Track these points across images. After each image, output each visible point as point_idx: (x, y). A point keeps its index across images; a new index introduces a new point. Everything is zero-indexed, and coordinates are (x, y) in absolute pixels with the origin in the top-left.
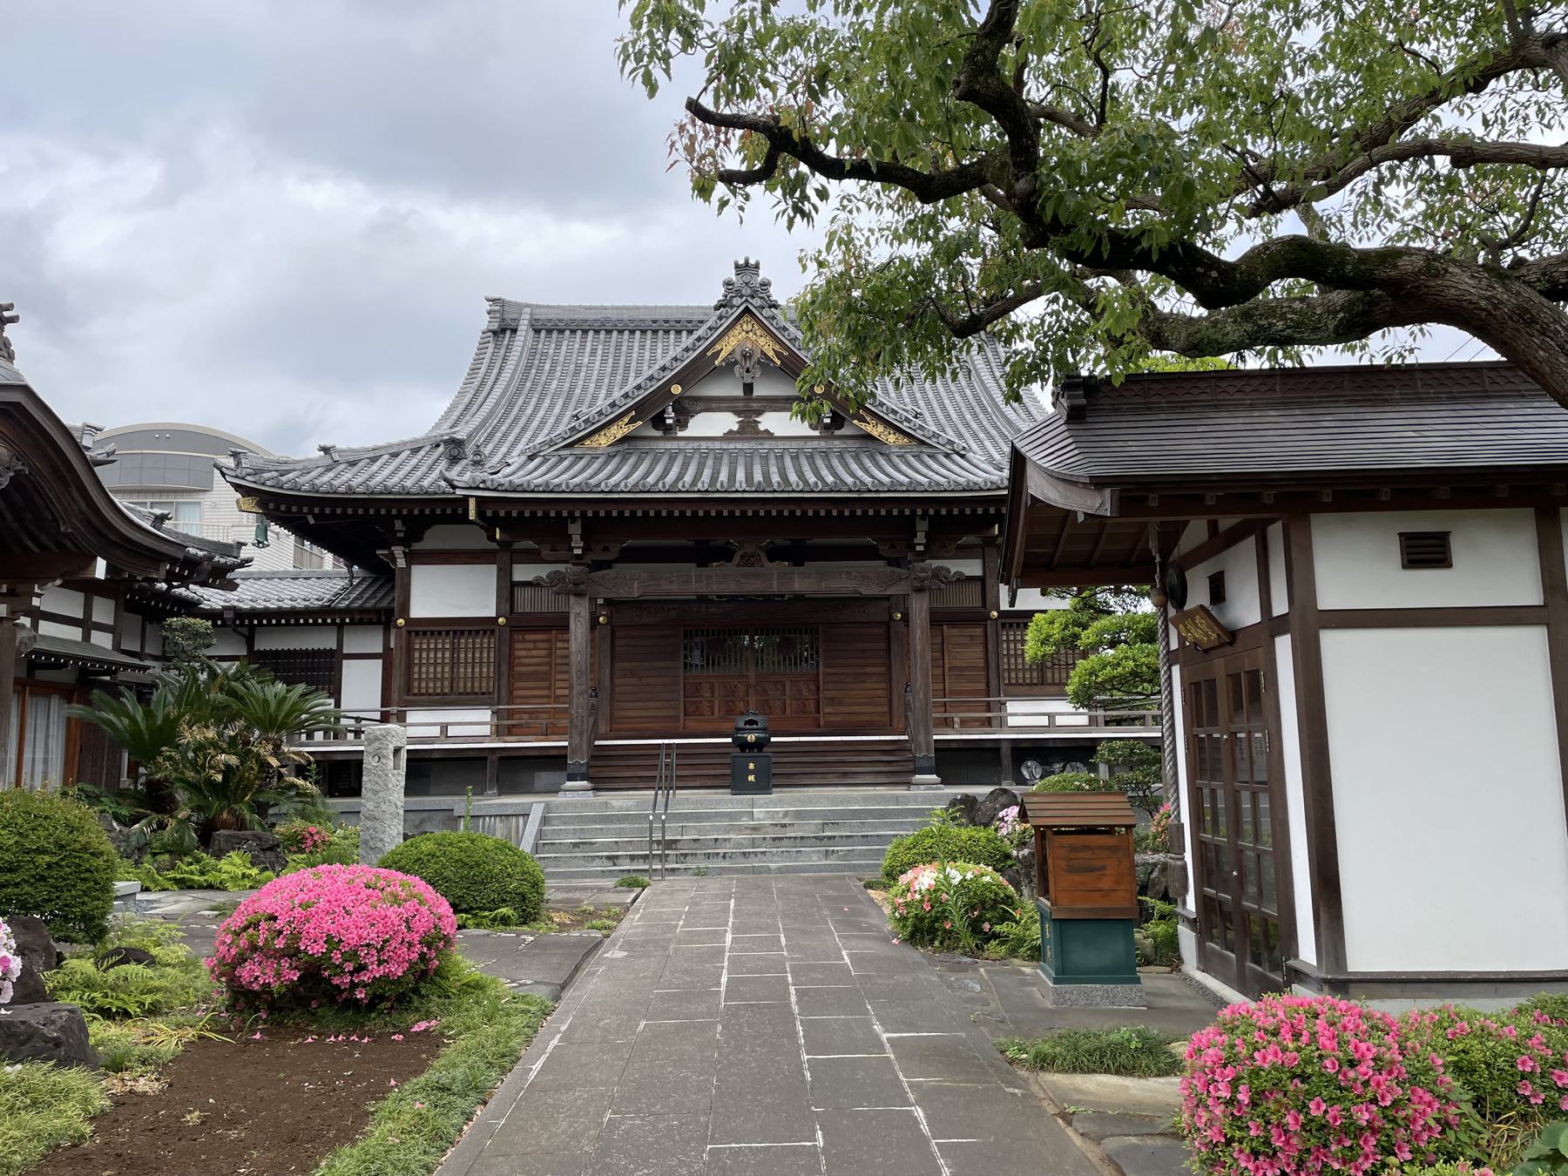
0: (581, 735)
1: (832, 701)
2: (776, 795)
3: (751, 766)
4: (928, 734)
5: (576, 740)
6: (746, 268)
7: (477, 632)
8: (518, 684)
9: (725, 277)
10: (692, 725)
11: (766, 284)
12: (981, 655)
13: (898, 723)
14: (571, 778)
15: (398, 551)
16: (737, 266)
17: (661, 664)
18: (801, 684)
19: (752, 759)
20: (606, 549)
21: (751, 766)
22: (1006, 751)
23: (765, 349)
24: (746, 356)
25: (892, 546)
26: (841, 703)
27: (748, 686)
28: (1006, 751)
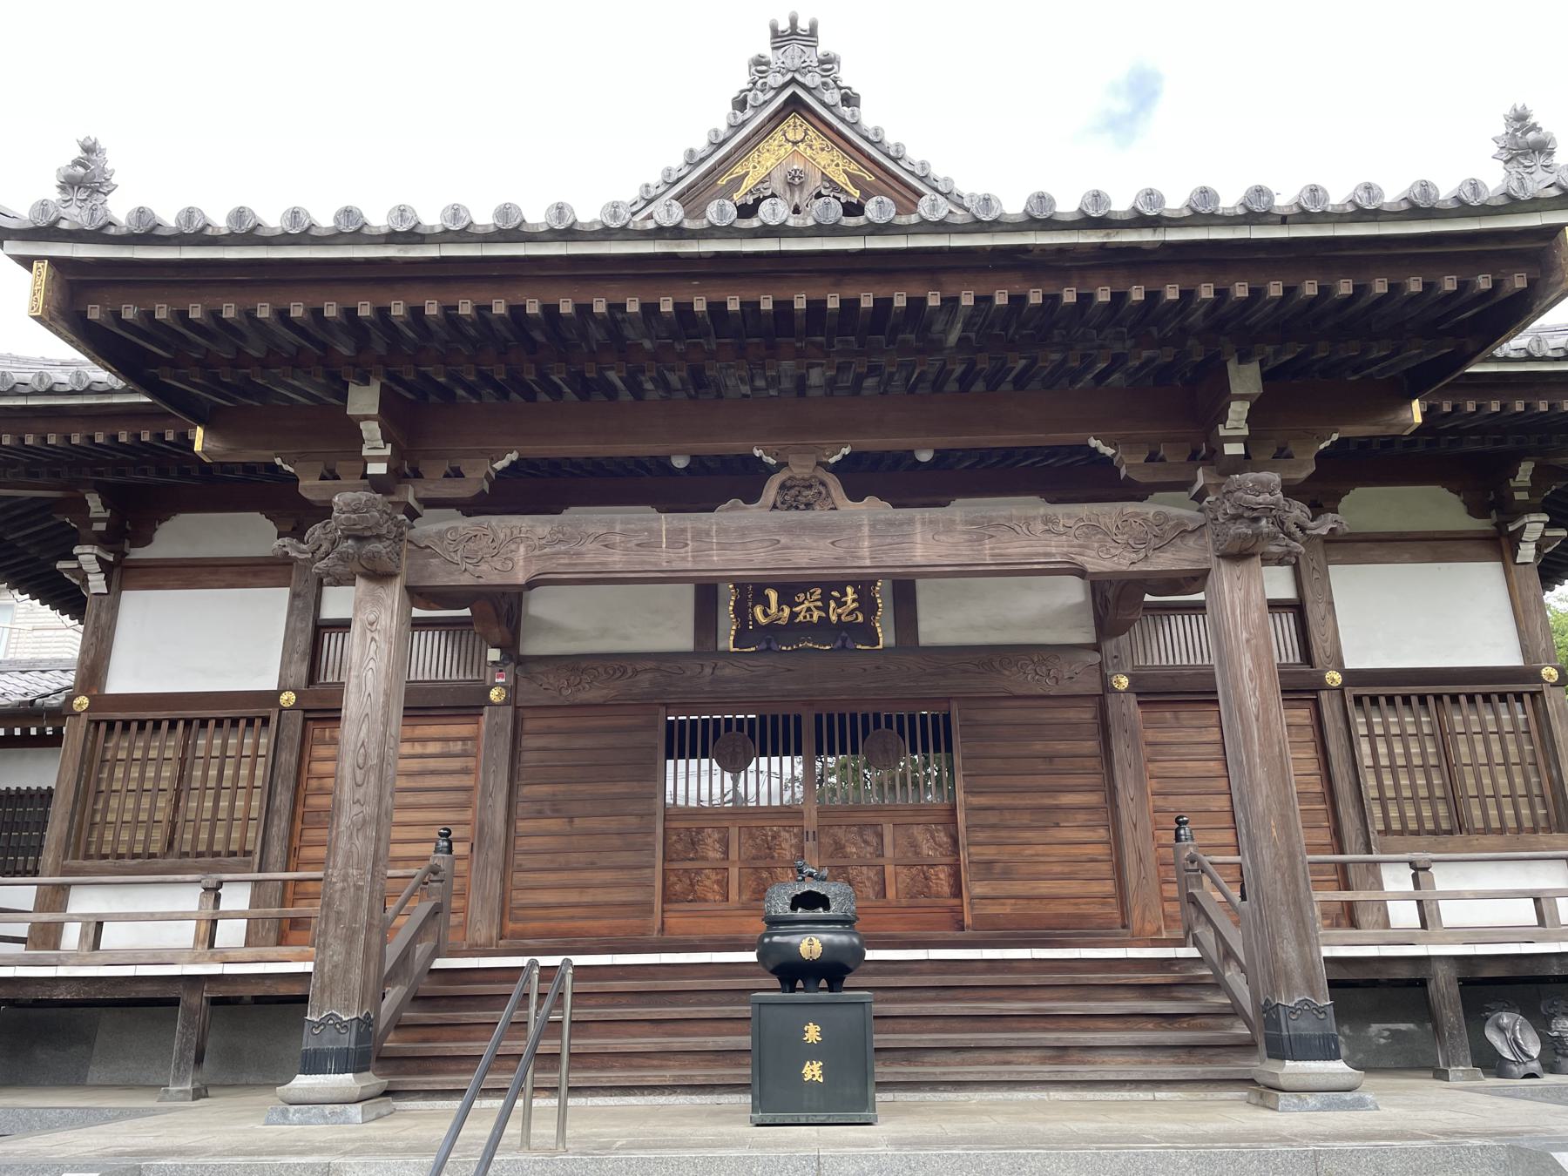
1: (986, 869)
3: (812, 1033)
4: (1305, 939)
5: (336, 952)
7: (235, 722)
9: (753, 54)
10: (679, 923)
11: (828, 61)
12: (1313, 767)
14: (314, 1063)
15: (87, 556)
16: (776, 34)
17: (620, 788)
18: (917, 832)
20: (457, 473)
21: (812, 1033)
22: (1444, 986)
23: (829, 172)
26: (1007, 875)
27: (802, 836)
28: (1444, 986)
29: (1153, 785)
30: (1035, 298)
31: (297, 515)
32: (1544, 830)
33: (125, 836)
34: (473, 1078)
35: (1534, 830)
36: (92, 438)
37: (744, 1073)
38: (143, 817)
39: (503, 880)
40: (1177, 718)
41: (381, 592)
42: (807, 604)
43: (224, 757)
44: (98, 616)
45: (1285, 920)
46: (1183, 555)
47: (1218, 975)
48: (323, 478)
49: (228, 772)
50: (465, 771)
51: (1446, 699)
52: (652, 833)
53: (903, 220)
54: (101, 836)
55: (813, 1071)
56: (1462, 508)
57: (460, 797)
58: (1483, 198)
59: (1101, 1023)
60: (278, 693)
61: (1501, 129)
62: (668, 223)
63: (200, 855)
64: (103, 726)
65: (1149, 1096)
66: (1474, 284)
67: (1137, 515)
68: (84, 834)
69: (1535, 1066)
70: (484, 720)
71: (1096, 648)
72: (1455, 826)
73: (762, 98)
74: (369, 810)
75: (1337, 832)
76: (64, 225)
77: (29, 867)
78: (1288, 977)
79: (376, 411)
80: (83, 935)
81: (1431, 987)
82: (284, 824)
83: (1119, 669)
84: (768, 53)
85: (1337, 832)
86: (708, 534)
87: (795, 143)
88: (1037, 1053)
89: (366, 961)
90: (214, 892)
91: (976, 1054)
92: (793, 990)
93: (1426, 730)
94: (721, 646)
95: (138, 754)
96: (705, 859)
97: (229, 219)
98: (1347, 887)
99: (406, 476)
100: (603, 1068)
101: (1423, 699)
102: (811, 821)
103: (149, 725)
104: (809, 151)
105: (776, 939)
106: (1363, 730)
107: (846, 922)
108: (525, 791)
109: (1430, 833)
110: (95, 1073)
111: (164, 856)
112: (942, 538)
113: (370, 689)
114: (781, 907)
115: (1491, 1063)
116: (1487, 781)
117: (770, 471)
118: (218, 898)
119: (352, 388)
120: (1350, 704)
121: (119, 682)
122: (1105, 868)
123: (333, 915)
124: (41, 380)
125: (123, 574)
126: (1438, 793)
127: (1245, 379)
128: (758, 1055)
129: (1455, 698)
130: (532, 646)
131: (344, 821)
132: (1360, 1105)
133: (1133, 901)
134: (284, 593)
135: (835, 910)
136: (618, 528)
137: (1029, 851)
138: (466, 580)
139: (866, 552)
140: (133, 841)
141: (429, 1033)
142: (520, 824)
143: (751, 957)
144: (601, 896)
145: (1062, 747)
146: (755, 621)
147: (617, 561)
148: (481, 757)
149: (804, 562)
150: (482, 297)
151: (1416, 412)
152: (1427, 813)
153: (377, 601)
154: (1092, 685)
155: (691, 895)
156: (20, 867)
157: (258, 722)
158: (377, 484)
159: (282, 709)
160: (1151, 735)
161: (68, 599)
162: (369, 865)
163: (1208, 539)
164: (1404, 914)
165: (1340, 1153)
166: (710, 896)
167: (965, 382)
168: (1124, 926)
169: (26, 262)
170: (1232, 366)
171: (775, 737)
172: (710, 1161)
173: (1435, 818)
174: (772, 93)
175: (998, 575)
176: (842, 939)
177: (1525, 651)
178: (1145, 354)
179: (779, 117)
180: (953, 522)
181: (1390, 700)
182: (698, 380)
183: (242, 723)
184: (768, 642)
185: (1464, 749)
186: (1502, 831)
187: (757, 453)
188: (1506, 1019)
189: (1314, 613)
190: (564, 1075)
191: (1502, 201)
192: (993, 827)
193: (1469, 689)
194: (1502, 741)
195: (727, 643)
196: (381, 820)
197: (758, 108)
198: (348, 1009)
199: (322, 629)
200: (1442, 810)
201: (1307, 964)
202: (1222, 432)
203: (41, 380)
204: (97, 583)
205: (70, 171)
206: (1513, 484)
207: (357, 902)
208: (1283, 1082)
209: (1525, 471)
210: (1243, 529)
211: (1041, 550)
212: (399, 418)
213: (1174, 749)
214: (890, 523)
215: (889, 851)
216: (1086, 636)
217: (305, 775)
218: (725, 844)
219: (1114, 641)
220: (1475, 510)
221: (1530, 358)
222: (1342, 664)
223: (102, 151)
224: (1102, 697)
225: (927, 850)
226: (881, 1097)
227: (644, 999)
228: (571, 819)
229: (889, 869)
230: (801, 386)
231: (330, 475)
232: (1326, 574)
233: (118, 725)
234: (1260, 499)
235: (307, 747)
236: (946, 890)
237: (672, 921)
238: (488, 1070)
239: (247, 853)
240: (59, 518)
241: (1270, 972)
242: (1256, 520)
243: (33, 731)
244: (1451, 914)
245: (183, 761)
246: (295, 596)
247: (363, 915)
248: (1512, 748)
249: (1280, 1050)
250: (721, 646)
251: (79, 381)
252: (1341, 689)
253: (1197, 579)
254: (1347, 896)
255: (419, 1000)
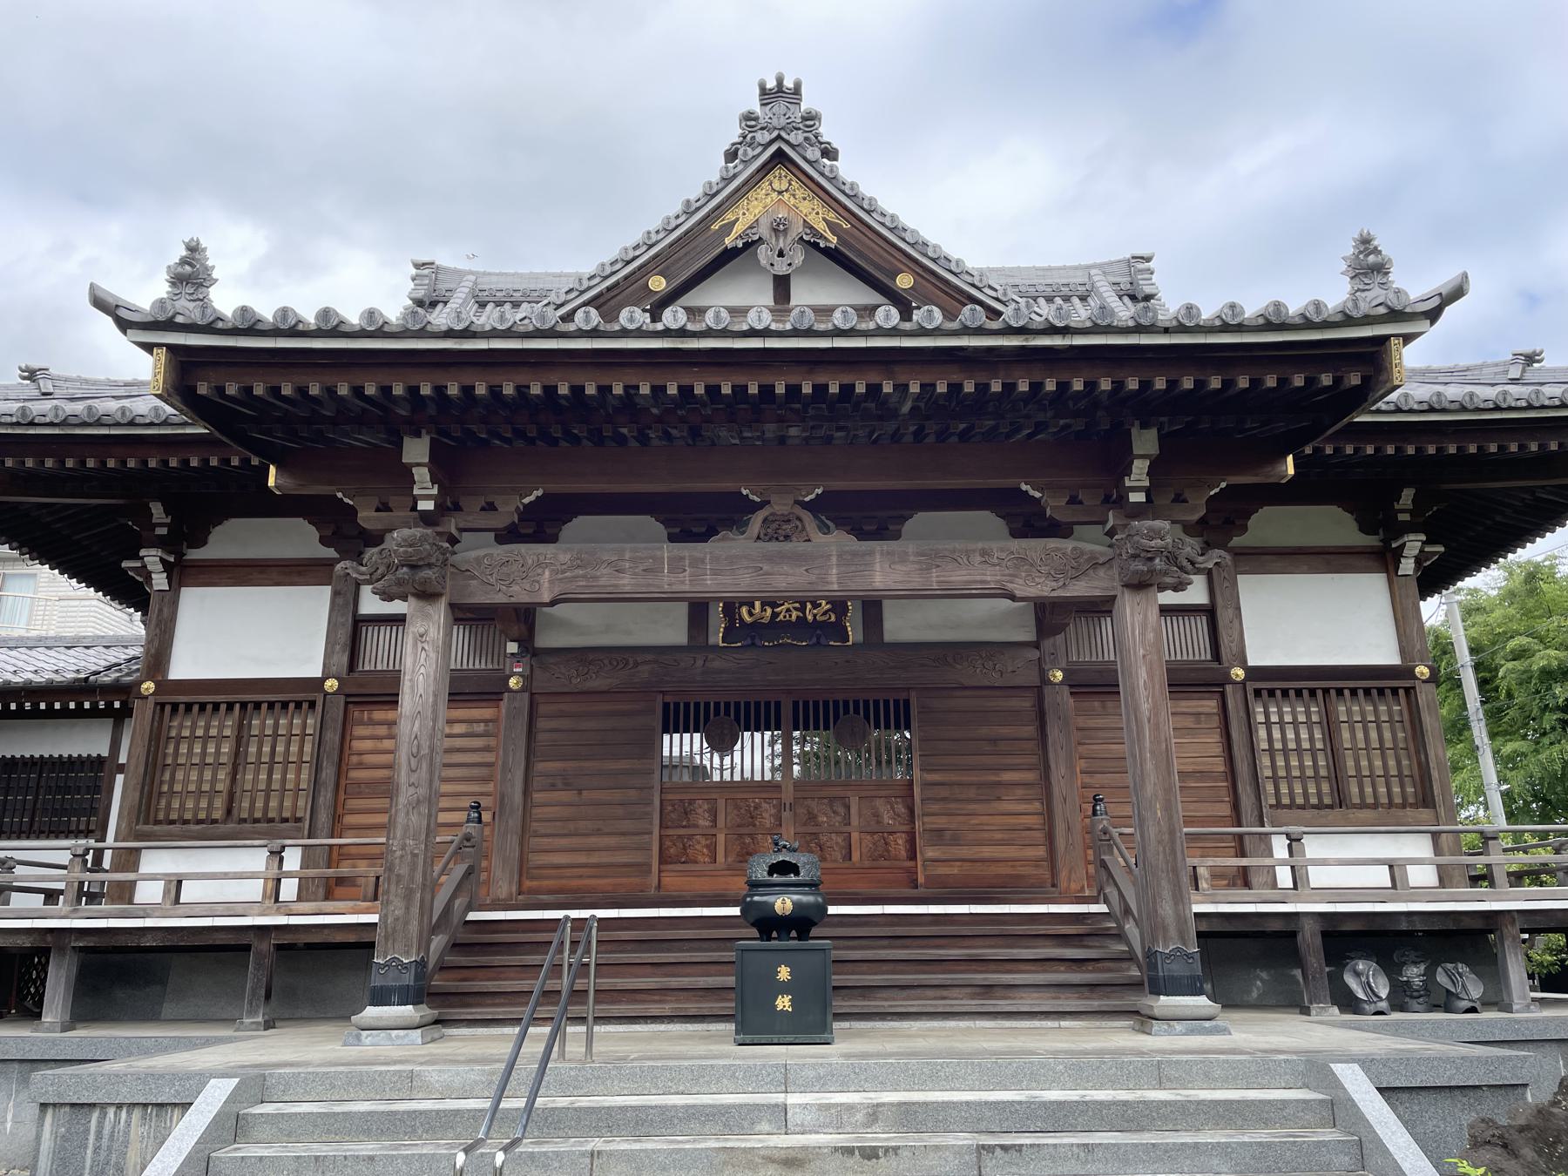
0: (408, 897)
1: (938, 836)
2: (851, 1044)
3: (784, 973)
4: (1180, 900)
5: (397, 906)
6: (774, 94)
8: (353, 803)
9: (744, 110)
10: (674, 881)
11: (811, 118)
12: (1218, 750)
13: (1075, 873)
14: (381, 997)
15: (152, 558)
16: (764, 91)
18: (880, 804)
19: (785, 956)
20: (490, 507)
21: (784, 973)
22: (1310, 938)
24: (779, 229)
25: (1073, 500)
26: (956, 841)
27: (780, 807)
28: (1310, 938)
29: (1082, 764)
30: (969, 387)
31: (348, 536)
32: (1411, 805)
33: (190, 804)
34: (528, 1009)
35: (1403, 806)
36: (165, 463)
37: (729, 1006)
38: (206, 787)
39: (521, 844)
40: (1104, 707)
41: (430, 609)
42: (787, 605)
43: (275, 735)
44: (160, 610)
45: (1164, 883)
46: (1096, 583)
47: (1120, 927)
48: (378, 510)
49: (280, 749)
50: (487, 749)
51: (1333, 692)
52: (650, 803)
53: (863, 326)
54: (169, 804)
55: (783, 1003)
56: (1354, 526)
57: (484, 771)
58: (1324, 316)
59: (1022, 966)
60: (322, 680)
61: (1349, 250)
62: (674, 327)
63: (256, 821)
64: (168, 709)
65: (1055, 1024)
66: (1319, 380)
67: (1058, 549)
68: (154, 802)
69: (1383, 1005)
70: (504, 704)
71: (1036, 645)
72: (1339, 803)
73: (751, 153)
74: (422, 791)
75: (1236, 806)
76: (179, 319)
77: (82, 827)
78: (1165, 929)
79: (426, 460)
80: (166, 892)
81: (1299, 937)
82: (330, 795)
83: (1056, 666)
84: (757, 109)
85: (1236, 806)
86: (703, 561)
87: (780, 193)
88: (969, 990)
89: (422, 914)
90: (277, 855)
91: (918, 992)
92: (769, 939)
93: (1315, 718)
94: (712, 641)
95: (199, 733)
96: (696, 826)
97: (317, 318)
98: (1243, 855)
99: (449, 509)
100: (613, 1002)
101: (1313, 692)
102: (788, 795)
103: (209, 707)
104: (792, 200)
105: (756, 898)
106: (1261, 718)
107: (812, 885)
108: (540, 767)
109: (1314, 807)
110: (168, 1009)
111: (225, 822)
112: (897, 567)
113: (421, 691)
114: (761, 874)
115: (1349, 1003)
116: (1364, 763)
117: (757, 507)
118: (281, 859)
119: (407, 440)
120: (1251, 696)
121: (182, 668)
122: (1039, 835)
123: (394, 878)
124: (123, 414)
125: (183, 573)
126: (1323, 772)
127: (1145, 442)
128: (739, 992)
129: (1340, 692)
130: (544, 640)
131: (402, 800)
132: (1224, 1031)
133: (1060, 863)
134: (326, 591)
135: (804, 876)
136: (627, 556)
137: (975, 821)
138: (500, 599)
139: (834, 579)
140: (197, 809)
141: (466, 973)
142: (535, 795)
143: (736, 911)
144: (605, 858)
145: (1005, 731)
146: (741, 620)
147: (626, 583)
148: (501, 736)
149: (783, 586)
150: (522, 379)
151: (1290, 467)
152: (1312, 790)
153: (427, 617)
154: (1032, 678)
155: (685, 857)
156: (73, 827)
157: (305, 706)
158: (427, 519)
159: (326, 694)
160: (1081, 722)
161: (129, 592)
162: (423, 837)
163: (1115, 571)
164: (1284, 877)
165: (1177, 1062)
166: (700, 858)
167: (919, 435)
168: (1053, 885)
169: (148, 347)
170: (1135, 431)
171: (759, 717)
172: (703, 1068)
173: (1319, 794)
174: (760, 149)
175: (949, 583)
176: (808, 899)
177: (1403, 652)
178: (1062, 422)
179: (766, 169)
180: (906, 553)
181: (1285, 693)
182: (695, 433)
183: (292, 706)
184: (753, 638)
185: (1346, 735)
186: (1375, 806)
187: (745, 492)
188: (1361, 966)
189: (1223, 616)
190: (590, 1008)
191: (1339, 318)
192: (944, 799)
193: (1352, 684)
194: (1379, 728)
195: (717, 637)
196: (432, 799)
197: (746, 163)
198: (407, 954)
199: (360, 623)
200: (1325, 788)
201: (1181, 919)
202: (1128, 484)
203: (123, 414)
204: (160, 581)
205: (180, 269)
206: (1397, 507)
207: (413, 868)
208: (1157, 1012)
209: (1407, 497)
210: (1140, 566)
211: (978, 578)
212: (443, 465)
213: (1101, 734)
214: (854, 554)
215: (855, 820)
216: (1027, 634)
217: (347, 751)
218: (714, 814)
219: (1051, 640)
220: (1365, 528)
221: (1399, 410)
222: (1245, 661)
223: (204, 250)
224: (1040, 688)
225: (887, 819)
226: (836, 1025)
227: (644, 946)
228: (580, 791)
229: (855, 836)
230: (782, 440)
231: (384, 507)
232: (1235, 584)
233: (182, 707)
234: (1153, 543)
235: (348, 727)
236: (903, 853)
237: (666, 880)
238: (538, 1004)
239: (298, 820)
240: (122, 521)
241: (1154, 928)
242: (1151, 559)
243: (87, 705)
244: (1318, 877)
245: (239, 739)
246: (335, 594)
247: (419, 877)
248: (1387, 735)
249: (1159, 987)
250: (712, 641)
251: (157, 416)
252: (1243, 683)
253: (1100, 608)
254: (1244, 862)
255: (456, 946)
